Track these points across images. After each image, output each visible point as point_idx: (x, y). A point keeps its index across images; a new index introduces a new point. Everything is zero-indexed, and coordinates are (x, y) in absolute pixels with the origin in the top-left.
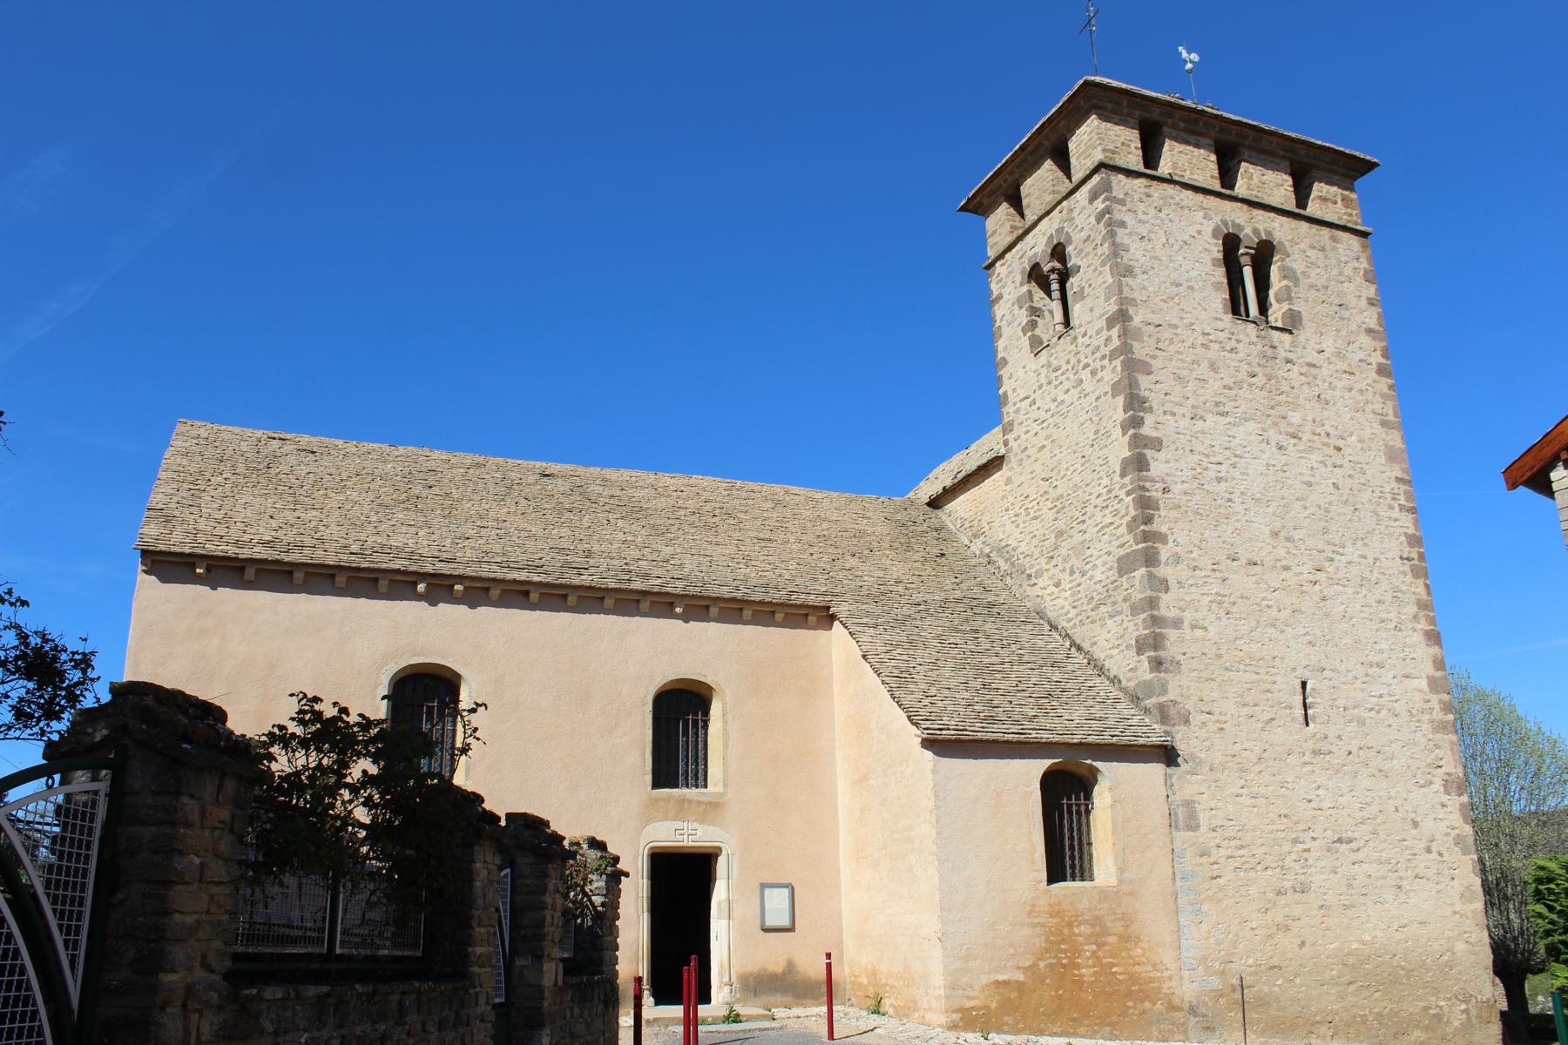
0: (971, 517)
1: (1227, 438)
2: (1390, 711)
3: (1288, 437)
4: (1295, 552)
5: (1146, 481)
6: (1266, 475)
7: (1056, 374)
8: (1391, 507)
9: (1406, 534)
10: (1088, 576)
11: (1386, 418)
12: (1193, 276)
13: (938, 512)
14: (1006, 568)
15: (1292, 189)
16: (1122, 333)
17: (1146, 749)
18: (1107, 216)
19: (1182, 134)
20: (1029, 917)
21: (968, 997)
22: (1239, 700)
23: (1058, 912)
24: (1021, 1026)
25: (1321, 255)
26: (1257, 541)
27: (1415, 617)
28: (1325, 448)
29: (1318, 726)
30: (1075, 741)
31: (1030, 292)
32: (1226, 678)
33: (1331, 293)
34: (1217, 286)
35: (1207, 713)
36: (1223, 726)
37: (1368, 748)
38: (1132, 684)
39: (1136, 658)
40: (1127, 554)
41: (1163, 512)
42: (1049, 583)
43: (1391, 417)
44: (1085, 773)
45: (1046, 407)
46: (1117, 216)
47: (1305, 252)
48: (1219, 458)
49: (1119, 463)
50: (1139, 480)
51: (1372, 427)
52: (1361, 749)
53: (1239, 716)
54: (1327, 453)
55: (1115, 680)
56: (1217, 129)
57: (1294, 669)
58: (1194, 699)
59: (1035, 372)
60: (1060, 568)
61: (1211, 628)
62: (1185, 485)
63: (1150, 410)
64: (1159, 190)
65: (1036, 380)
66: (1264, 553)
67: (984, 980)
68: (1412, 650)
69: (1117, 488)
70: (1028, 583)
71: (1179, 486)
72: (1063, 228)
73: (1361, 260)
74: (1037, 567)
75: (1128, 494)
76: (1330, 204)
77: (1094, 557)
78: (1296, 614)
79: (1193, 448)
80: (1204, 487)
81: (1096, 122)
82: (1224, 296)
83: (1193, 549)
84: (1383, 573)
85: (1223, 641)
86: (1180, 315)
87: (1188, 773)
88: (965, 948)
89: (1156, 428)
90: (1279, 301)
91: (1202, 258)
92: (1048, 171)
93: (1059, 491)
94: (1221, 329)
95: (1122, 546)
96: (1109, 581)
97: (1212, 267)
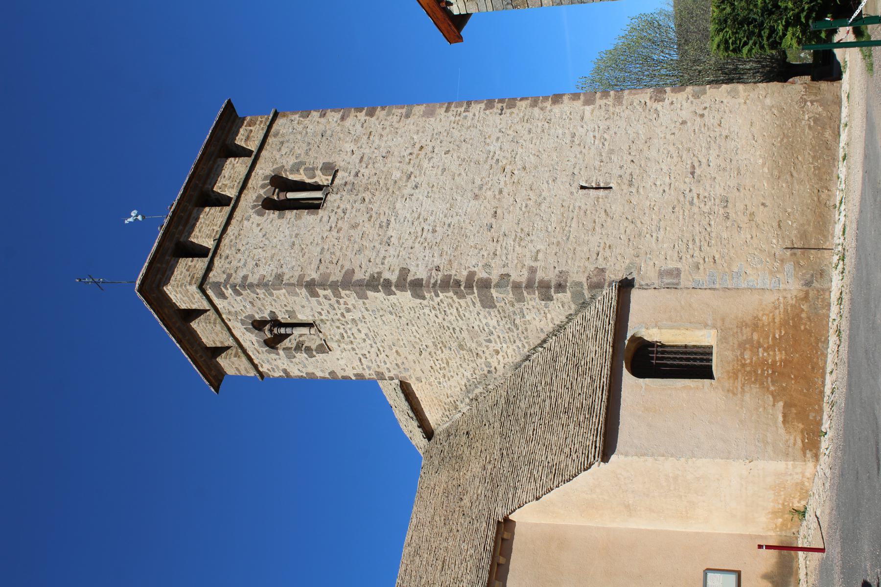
0: (441, 409)
3: (410, 180)
4: (490, 184)
6: (434, 198)
8: (465, 117)
9: (484, 110)
10: (493, 330)
11: (404, 114)
13: (436, 433)
14: (482, 388)
16: (322, 287)
17: (620, 301)
18: (237, 288)
19: (187, 228)
20: (737, 394)
21: (795, 444)
22: (590, 233)
23: (734, 373)
24: (816, 407)
25: (286, 145)
26: (480, 210)
27: (542, 109)
28: (420, 157)
30: (611, 350)
31: (284, 349)
32: (574, 241)
34: (298, 218)
36: (607, 246)
37: (630, 149)
38: (573, 306)
40: (480, 300)
41: (453, 272)
42: (495, 358)
43: (404, 111)
45: (369, 347)
46: (239, 281)
48: (419, 229)
49: (414, 299)
50: (428, 286)
53: (602, 234)
55: (569, 318)
57: (572, 193)
58: (587, 263)
59: (342, 352)
60: (485, 349)
61: (538, 247)
62: (435, 255)
63: (380, 273)
64: (225, 249)
66: (488, 206)
67: (782, 431)
68: (565, 113)
70: (494, 373)
73: (293, 118)
74: (483, 366)
75: (437, 296)
78: (534, 188)
81: (169, 287)
82: (306, 214)
83: (481, 254)
84: (510, 127)
86: (315, 245)
87: (639, 273)
88: (757, 443)
89: (393, 271)
90: (314, 177)
93: (430, 344)
94: (328, 218)
95: (474, 304)
96: (498, 316)
97: (284, 219)
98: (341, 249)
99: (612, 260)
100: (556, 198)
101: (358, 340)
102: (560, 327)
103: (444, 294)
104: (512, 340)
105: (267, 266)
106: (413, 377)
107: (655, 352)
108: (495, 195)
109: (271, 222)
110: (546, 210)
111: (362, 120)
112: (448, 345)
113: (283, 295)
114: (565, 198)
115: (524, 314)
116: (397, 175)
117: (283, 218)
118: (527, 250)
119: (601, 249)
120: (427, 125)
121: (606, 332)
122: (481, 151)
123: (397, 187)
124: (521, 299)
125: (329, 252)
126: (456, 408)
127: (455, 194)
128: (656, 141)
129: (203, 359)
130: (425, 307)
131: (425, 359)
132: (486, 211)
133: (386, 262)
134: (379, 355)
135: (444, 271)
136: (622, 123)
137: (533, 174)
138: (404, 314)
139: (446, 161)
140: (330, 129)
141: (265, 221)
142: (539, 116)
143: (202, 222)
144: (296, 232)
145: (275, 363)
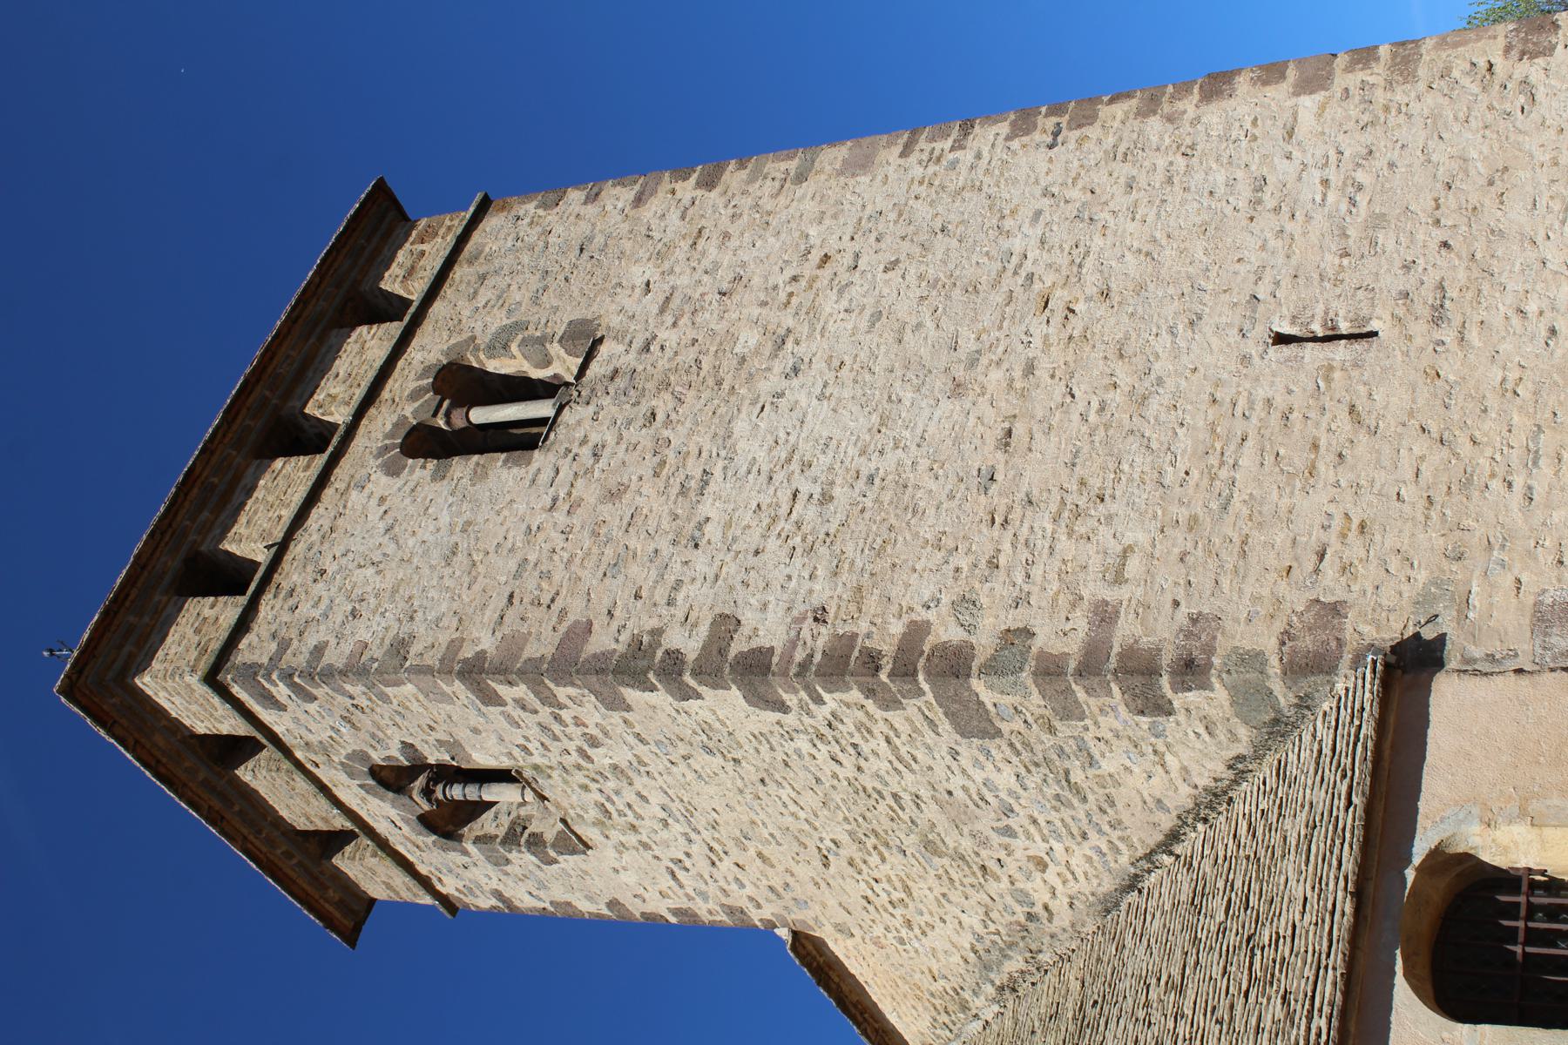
0: (926, 1009)
1: (751, 477)
2: (1358, 165)
3: (781, 354)
4: (1001, 349)
5: (790, 661)
6: (839, 400)
7: (615, 815)
8: (953, 165)
9: (1008, 138)
10: (1012, 801)
11: (792, 173)
12: (448, 519)
14: (1020, 959)
15: (375, 327)
16: (502, 678)
17: (1392, 719)
18: (297, 679)
19: (223, 517)
22: (1298, 485)
25: (490, 282)
26: (963, 428)
27: (1170, 119)
28: (817, 285)
29: (1378, 311)
30: (1348, 909)
31: (478, 840)
32: (1245, 511)
33: (557, 266)
34: (479, 475)
35: (1321, 560)
36: (1356, 522)
37: (1438, 207)
38: (1243, 732)
39: (1181, 717)
40: (946, 714)
41: (863, 627)
42: (1039, 880)
43: (792, 165)
44: (1440, 889)
45: (682, 840)
46: (301, 661)
47: (477, 309)
48: (784, 497)
49: (757, 711)
50: (785, 674)
51: (803, 197)
52: (1438, 221)
53: (1337, 485)
54: (826, 282)
55: (1239, 768)
56: (234, 453)
57: (1245, 359)
58: (1283, 588)
59: (620, 853)
60: (1002, 855)
61: (1128, 539)
62: (819, 573)
63: (657, 633)
64: (291, 574)
65: (635, 852)
66: (989, 414)
68: (1237, 124)
69: (811, 721)
70: (1045, 921)
71: (817, 587)
72: (342, 764)
73: (521, 213)
74: (1009, 900)
75: (819, 701)
76: (421, 263)
77: (969, 784)
78: (1128, 351)
79: (754, 547)
80: (832, 531)
81: (147, 679)
82: (500, 463)
83: (951, 566)
84: (1075, 180)
85: (1160, 512)
86: (505, 553)
87: (1462, 616)
89: (695, 625)
90: (547, 362)
91: (425, 498)
92: (255, 776)
93: (844, 838)
94: (552, 474)
95: (932, 724)
96: (1014, 759)
97: (445, 482)
98: (569, 562)
99: (1368, 574)
100: (1194, 378)
101: (647, 823)
102: (1215, 795)
103: (837, 695)
104: (1075, 831)
105: (378, 615)
106: (826, 922)
107: (1523, 913)
108: (1012, 380)
109: (413, 491)
110: (1163, 417)
111: (686, 201)
112: (894, 842)
113: (413, 700)
114: (1225, 376)
115: (1091, 757)
116: (749, 339)
117: (444, 477)
118: (1091, 548)
119: (1332, 537)
120: (848, 196)
121: (1338, 832)
122: (987, 254)
123: (744, 376)
124: (1071, 711)
125: (537, 574)
126: (964, 1007)
127: (898, 384)
128: (1524, 175)
129: (294, 861)
130: (794, 735)
131: (843, 878)
132: (981, 428)
133: (680, 597)
134: (718, 863)
135: (838, 621)
136: (1415, 135)
137: (1130, 310)
138: (742, 751)
139: (886, 291)
140: (601, 231)
141: (400, 489)
142: (1161, 138)
143: (260, 497)
144: (468, 516)
145: (467, 874)
